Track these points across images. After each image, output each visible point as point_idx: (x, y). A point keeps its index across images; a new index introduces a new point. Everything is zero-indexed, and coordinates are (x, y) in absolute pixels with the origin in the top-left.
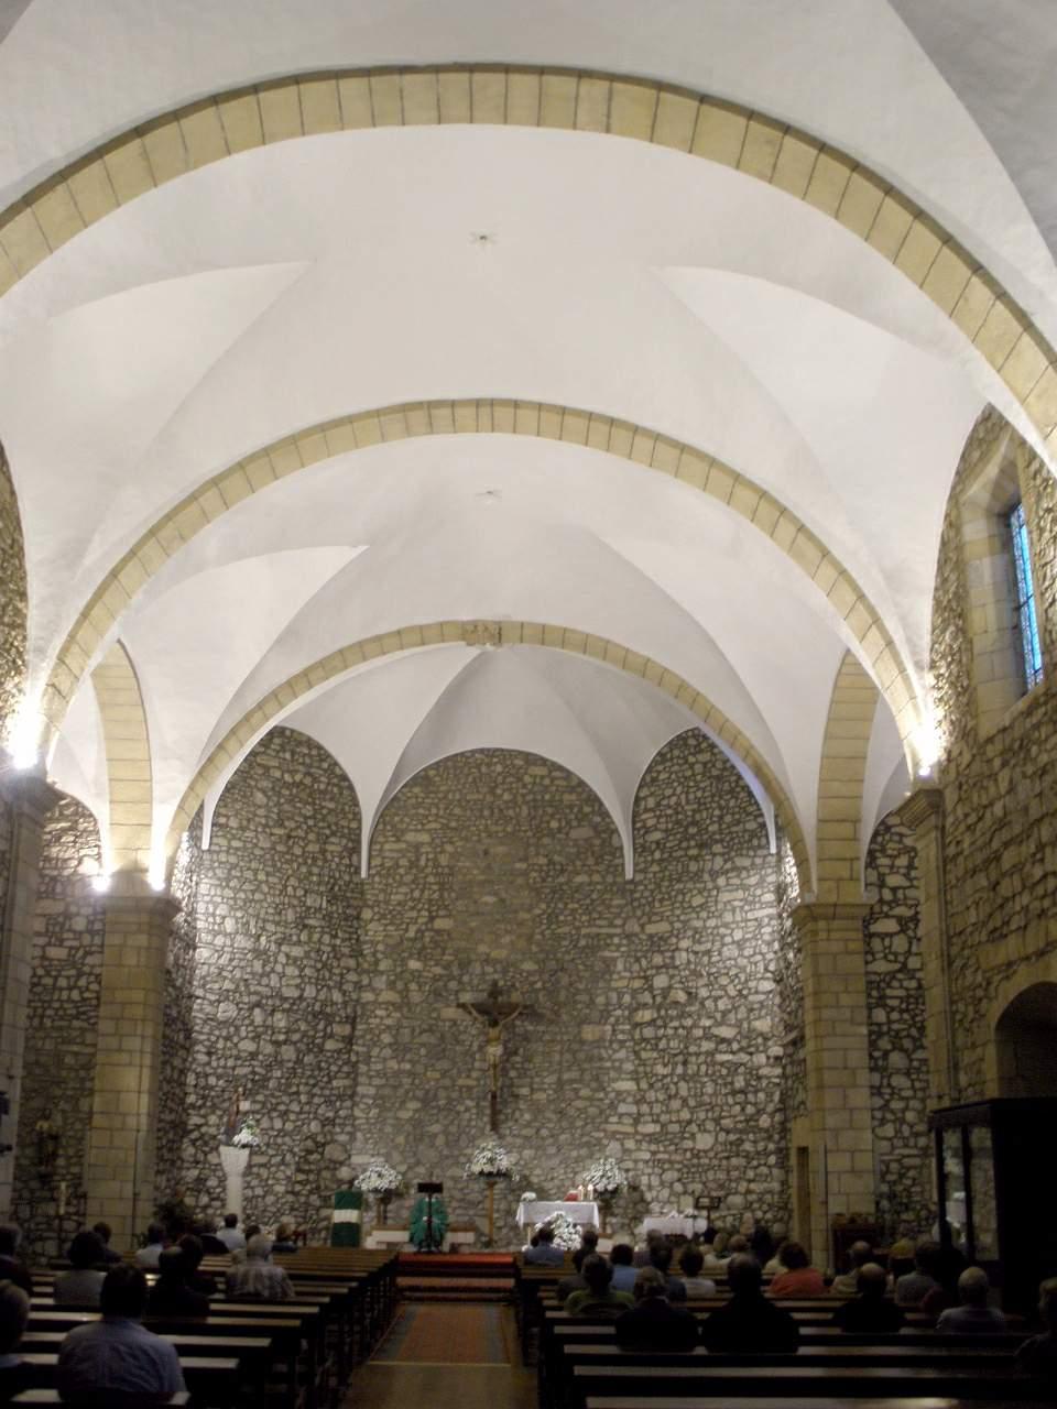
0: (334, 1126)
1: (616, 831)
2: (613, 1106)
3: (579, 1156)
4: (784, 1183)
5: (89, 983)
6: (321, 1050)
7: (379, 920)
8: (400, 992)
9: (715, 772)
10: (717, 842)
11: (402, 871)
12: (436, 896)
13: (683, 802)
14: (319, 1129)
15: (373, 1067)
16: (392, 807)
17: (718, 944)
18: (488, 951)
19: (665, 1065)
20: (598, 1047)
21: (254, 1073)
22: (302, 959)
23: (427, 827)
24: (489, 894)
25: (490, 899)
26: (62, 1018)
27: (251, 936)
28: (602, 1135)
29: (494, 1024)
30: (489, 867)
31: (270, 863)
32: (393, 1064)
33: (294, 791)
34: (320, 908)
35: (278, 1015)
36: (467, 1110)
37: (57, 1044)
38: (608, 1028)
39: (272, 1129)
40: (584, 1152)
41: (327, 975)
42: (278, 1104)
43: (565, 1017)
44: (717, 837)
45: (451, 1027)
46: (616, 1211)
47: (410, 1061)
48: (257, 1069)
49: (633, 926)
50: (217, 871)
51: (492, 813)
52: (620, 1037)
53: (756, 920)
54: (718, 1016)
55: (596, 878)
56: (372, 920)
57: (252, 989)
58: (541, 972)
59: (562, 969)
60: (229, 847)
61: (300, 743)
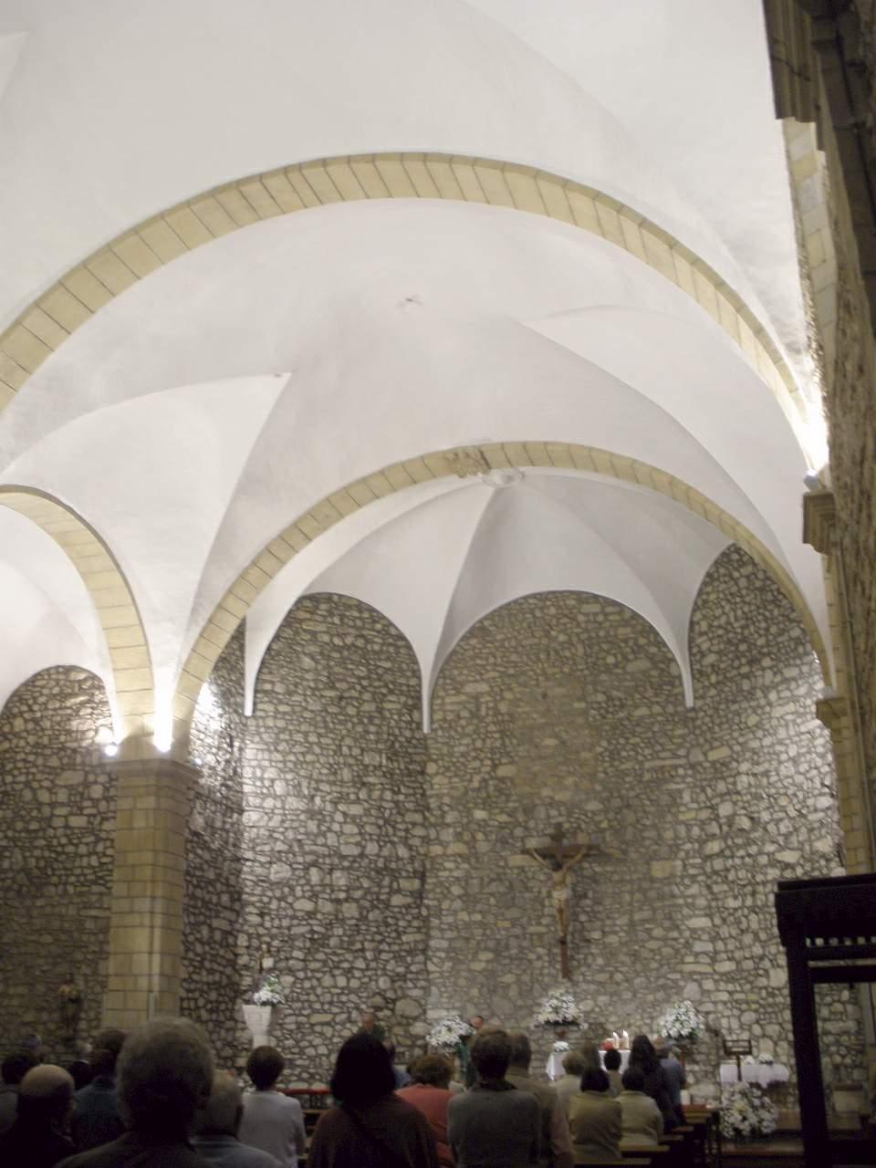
0: (405, 981)
1: (673, 660)
2: (688, 945)
3: (656, 1000)
4: (859, 1022)
5: (106, 848)
6: (387, 905)
7: (443, 774)
8: (466, 843)
9: (758, 584)
10: (765, 655)
11: (463, 722)
12: (498, 744)
13: (732, 620)
14: (388, 985)
15: (445, 919)
16: (450, 662)
17: (775, 763)
18: (551, 794)
19: (735, 898)
20: (670, 884)
21: (312, 932)
22: (360, 817)
23: (485, 677)
24: (550, 737)
25: (551, 742)
26: (83, 885)
27: (305, 797)
28: (678, 976)
29: (557, 867)
30: (549, 710)
31: (322, 725)
32: (464, 916)
33: (346, 653)
34: (381, 766)
35: (337, 874)
36: (539, 958)
37: (79, 909)
38: (679, 863)
39: (335, 987)
40: (660, 995)
41: (391, 831)
42: (340, 962)
43: (633, 855)
44: (765, 650)
45: (518, 874)
46: (698, 1058)
47: (481, 912)
48: (315, 928)
49: (697, 756)
50: (265, 736)
51: (549, 655)
52: (692, 871)
53: (809, 732)
54: (781, 840)
55: (657, 709)
56: (437, 774)
57: (307, 848)
58: (606, 811)
59: (628, 806)
60: (277, 711)
61: (350, 607)
